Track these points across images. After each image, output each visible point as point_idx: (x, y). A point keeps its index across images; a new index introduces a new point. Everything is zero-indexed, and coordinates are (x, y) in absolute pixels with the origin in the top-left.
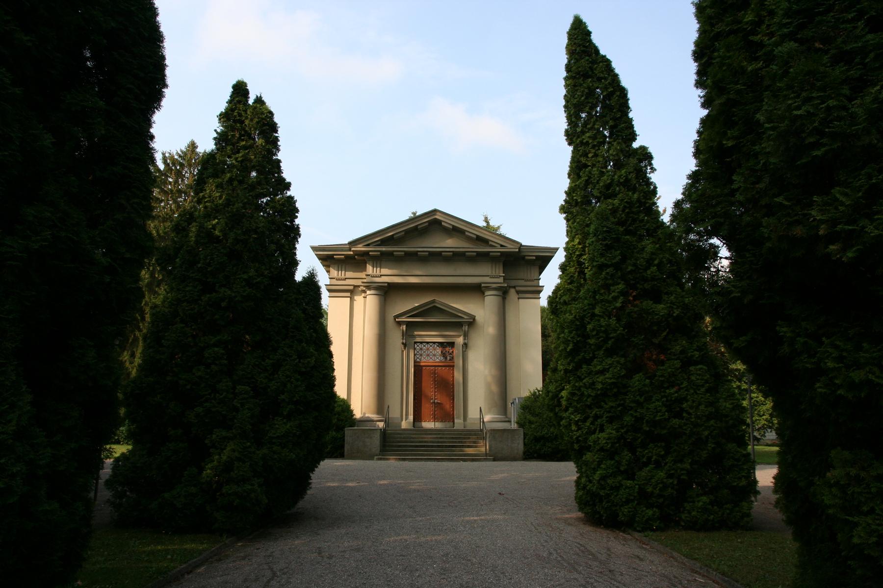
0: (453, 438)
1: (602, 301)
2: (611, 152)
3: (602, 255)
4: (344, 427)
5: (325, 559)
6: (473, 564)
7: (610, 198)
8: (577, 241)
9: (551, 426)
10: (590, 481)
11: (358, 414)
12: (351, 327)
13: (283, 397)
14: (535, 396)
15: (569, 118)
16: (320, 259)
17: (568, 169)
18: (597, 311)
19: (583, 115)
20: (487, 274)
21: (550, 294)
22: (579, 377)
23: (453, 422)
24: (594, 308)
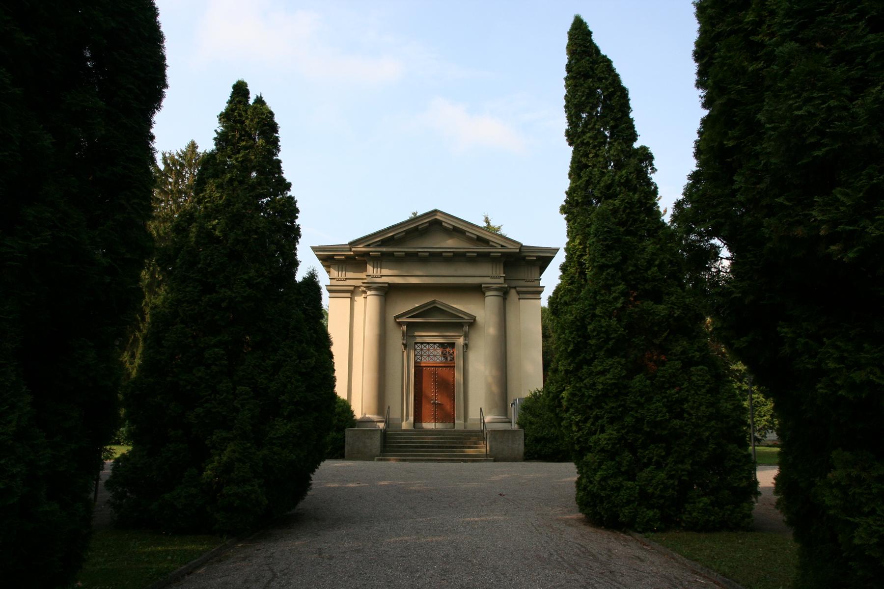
0: (453, 439)
1: (603, 301)
2: (611, 152)
3: (603, 255)
4: (344, 428)
5: (326, 560)
6: (473, 565)
7: (610, 198)
8: (577, 241)
9: (551, 427)
10: (591, 482)
11: (358, 415)
12: (352, 327)
13: (283, 397)
14: (535, 397)
15: (570, 118)
16: (320, 259)
17: (569, 169)
18: (598, 311)
19: (584, 115)
20: (487, 275)
21: (551, 294)
22: (580, 378)
23: (454, 422)
24: (595, 309)
